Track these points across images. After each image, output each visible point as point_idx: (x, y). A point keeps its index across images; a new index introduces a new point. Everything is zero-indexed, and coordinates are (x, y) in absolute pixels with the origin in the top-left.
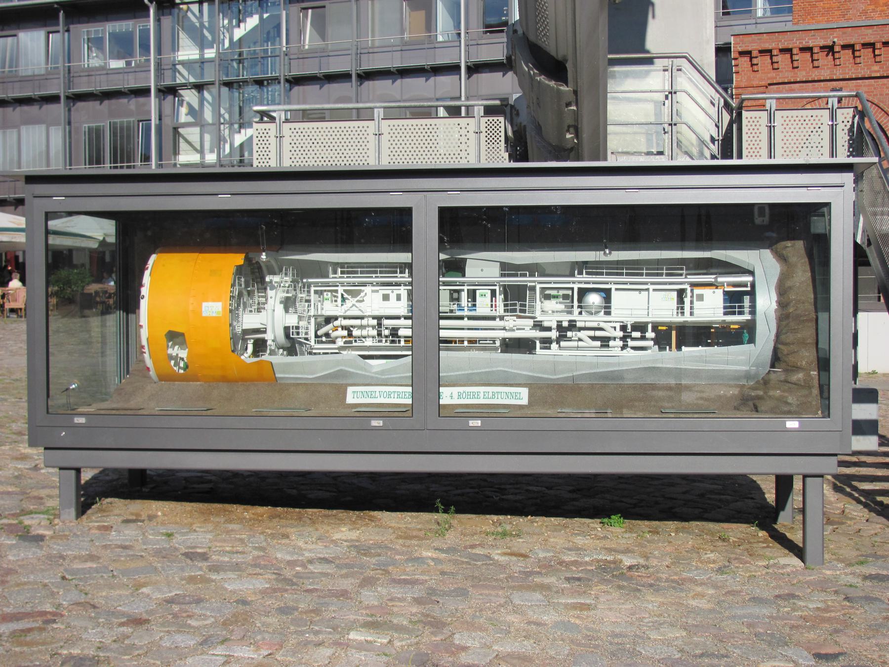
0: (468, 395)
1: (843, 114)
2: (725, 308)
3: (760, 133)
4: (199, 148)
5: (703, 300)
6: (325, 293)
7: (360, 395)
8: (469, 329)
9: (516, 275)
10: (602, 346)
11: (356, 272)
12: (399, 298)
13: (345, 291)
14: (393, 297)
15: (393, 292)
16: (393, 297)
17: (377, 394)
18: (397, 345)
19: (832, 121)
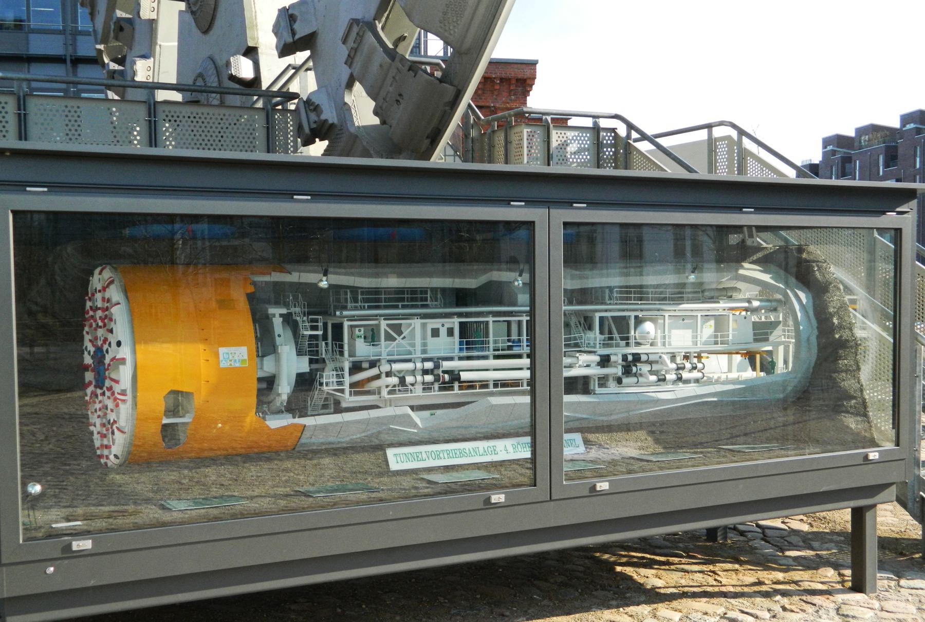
0: (462, 453)
1: (164, 111)
2: (755, 335)
3: (7, 122)
4: (659, 140)
5: (438, 336)
6: (357, 329)
7: (404, 458)
8: (494, 370)
9: (396, 307)
10: (659, 380)
11: (630, 299)
12: (450, 332)
13: (388, 325)
14: (443, 332)
15: (443, 325)
16: (443, 332)
17: (424, 456)
18: (409, 395)
19: (150, 116)
